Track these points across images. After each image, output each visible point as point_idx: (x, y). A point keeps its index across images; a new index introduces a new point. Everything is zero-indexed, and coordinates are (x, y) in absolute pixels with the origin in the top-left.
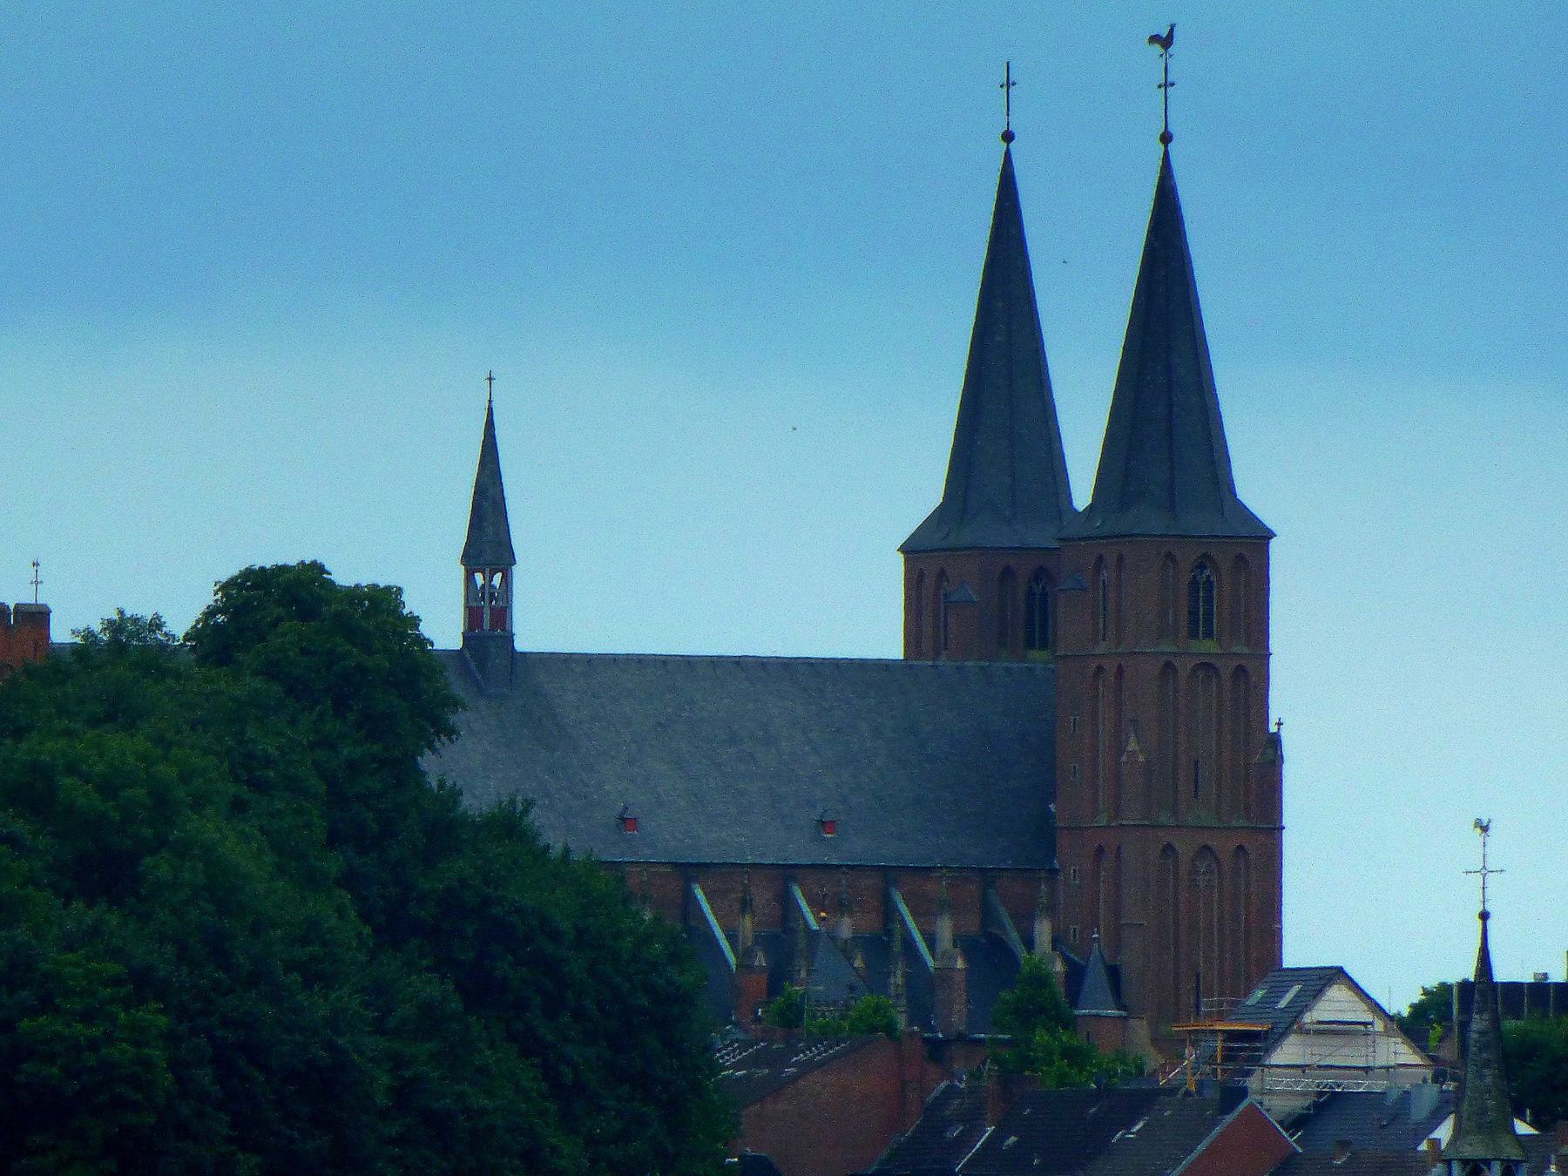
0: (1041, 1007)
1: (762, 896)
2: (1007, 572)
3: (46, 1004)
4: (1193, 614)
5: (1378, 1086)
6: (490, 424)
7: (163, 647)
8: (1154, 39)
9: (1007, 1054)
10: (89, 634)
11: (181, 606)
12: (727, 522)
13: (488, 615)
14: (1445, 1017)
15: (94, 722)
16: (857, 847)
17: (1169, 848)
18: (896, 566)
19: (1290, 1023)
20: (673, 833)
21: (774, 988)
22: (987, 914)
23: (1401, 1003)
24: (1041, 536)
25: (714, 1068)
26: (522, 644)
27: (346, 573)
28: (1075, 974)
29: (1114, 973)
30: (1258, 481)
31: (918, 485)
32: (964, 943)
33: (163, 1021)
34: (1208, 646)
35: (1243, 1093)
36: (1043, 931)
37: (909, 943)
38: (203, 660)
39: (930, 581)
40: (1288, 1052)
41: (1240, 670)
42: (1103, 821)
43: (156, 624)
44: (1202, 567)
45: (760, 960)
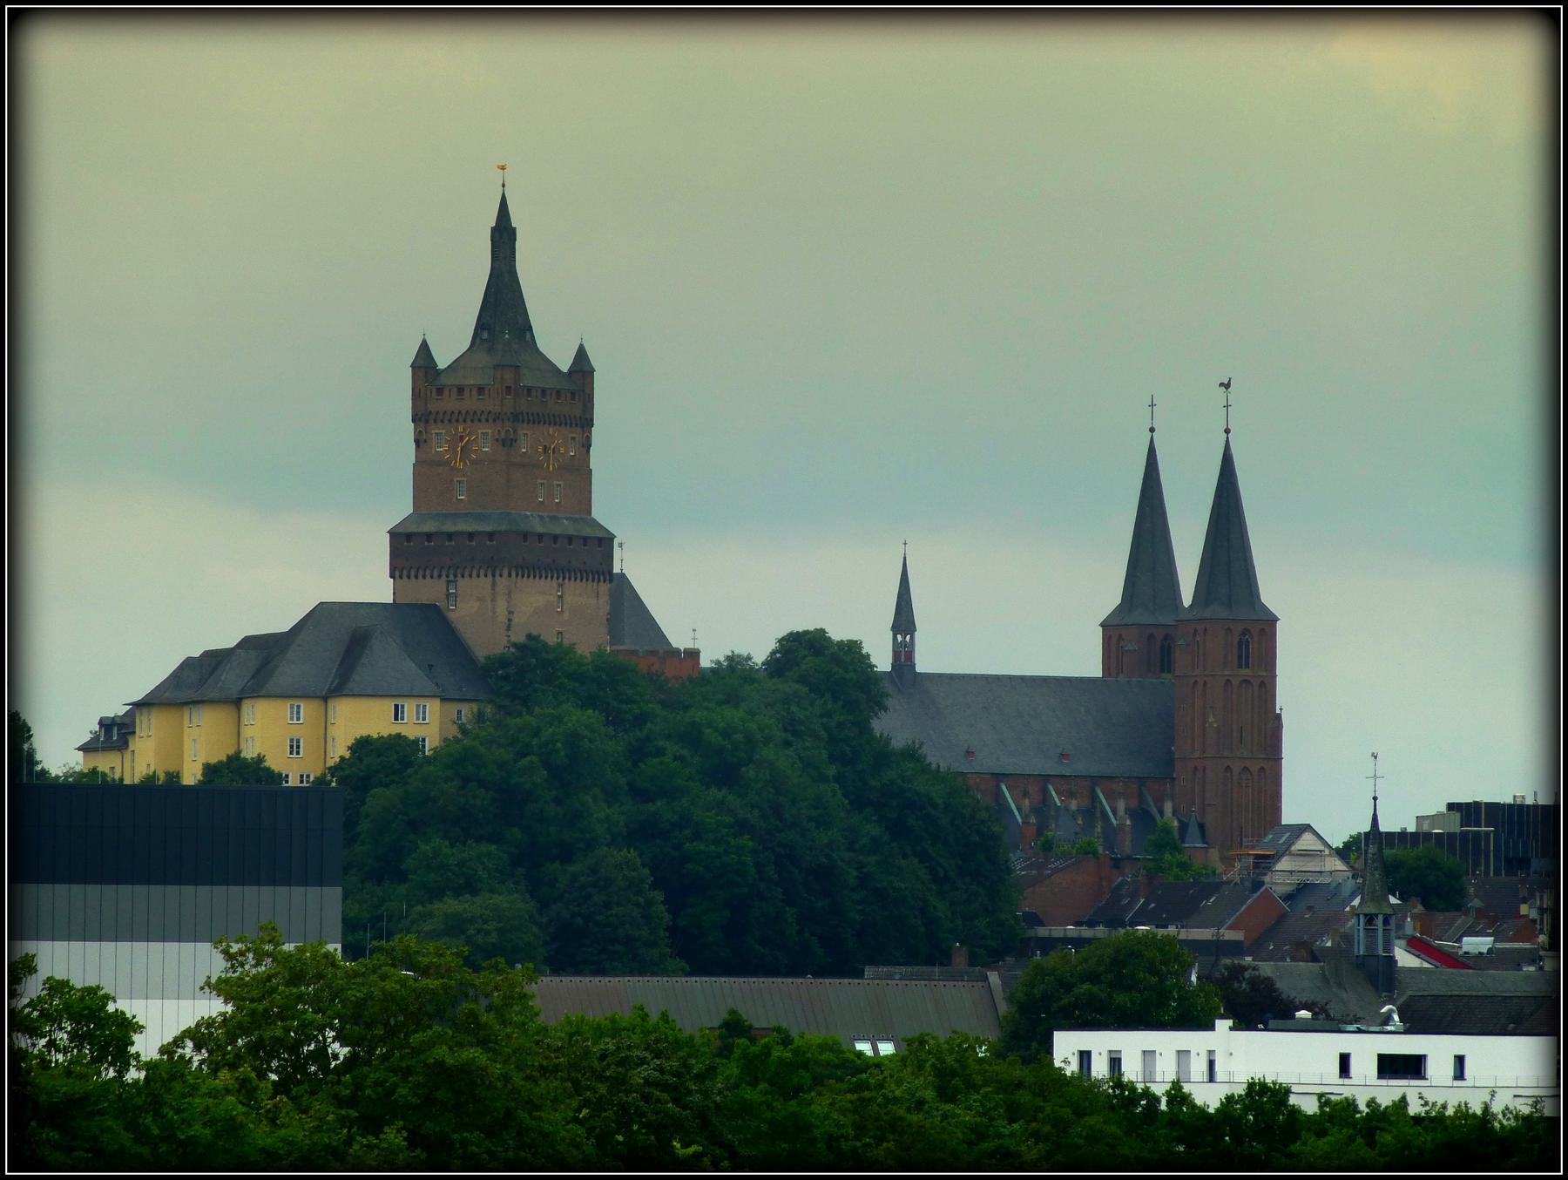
0: (1167, 843)
1: (1033, 789)
2: (1151, 636)
3: (697, 837)
4: (1240, 657)
5: (1327, 880)
6: (503, 236)
7: (752, 668)
8: (1221, 384)
9: (1151, 865)
10: (718, 662)
11: (760, 651)
12: (1020, 611)
13: (903, 655)
14: (1359, 848)
15: (720, 703)
16: (1079, 767)
17: (1228, 768)
18: (1098, 633)
19: (1285, 851)
20: (991, 759)
21: (1039, 833)
22: (1141, 799)
23: (1337, 842)
24: (1168, 619)
25: (1009, 871)
26: (918, 670)
27: (837, 634)
28: (1184, 827)
29: (1202, 827)
30: (1270, 595)
31: (1108, 592)
32: (1130, 812)
33: (751, 844)
34: (1245, 671)
35: (1262, 883)
36: (1168, 807)
37: (1104, 813)
38: (771, 676)
39: (1114, 639)
40: (1284, 864)
42: (1197, 755)
43: (749, 658)
45: (1033, 820)
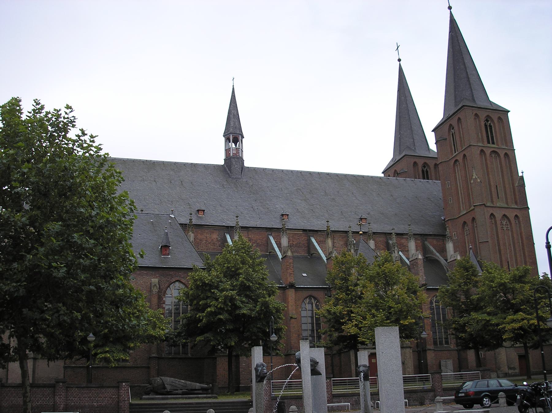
6: (233, 89)
41: (506, 154)
44: (487, 121)
